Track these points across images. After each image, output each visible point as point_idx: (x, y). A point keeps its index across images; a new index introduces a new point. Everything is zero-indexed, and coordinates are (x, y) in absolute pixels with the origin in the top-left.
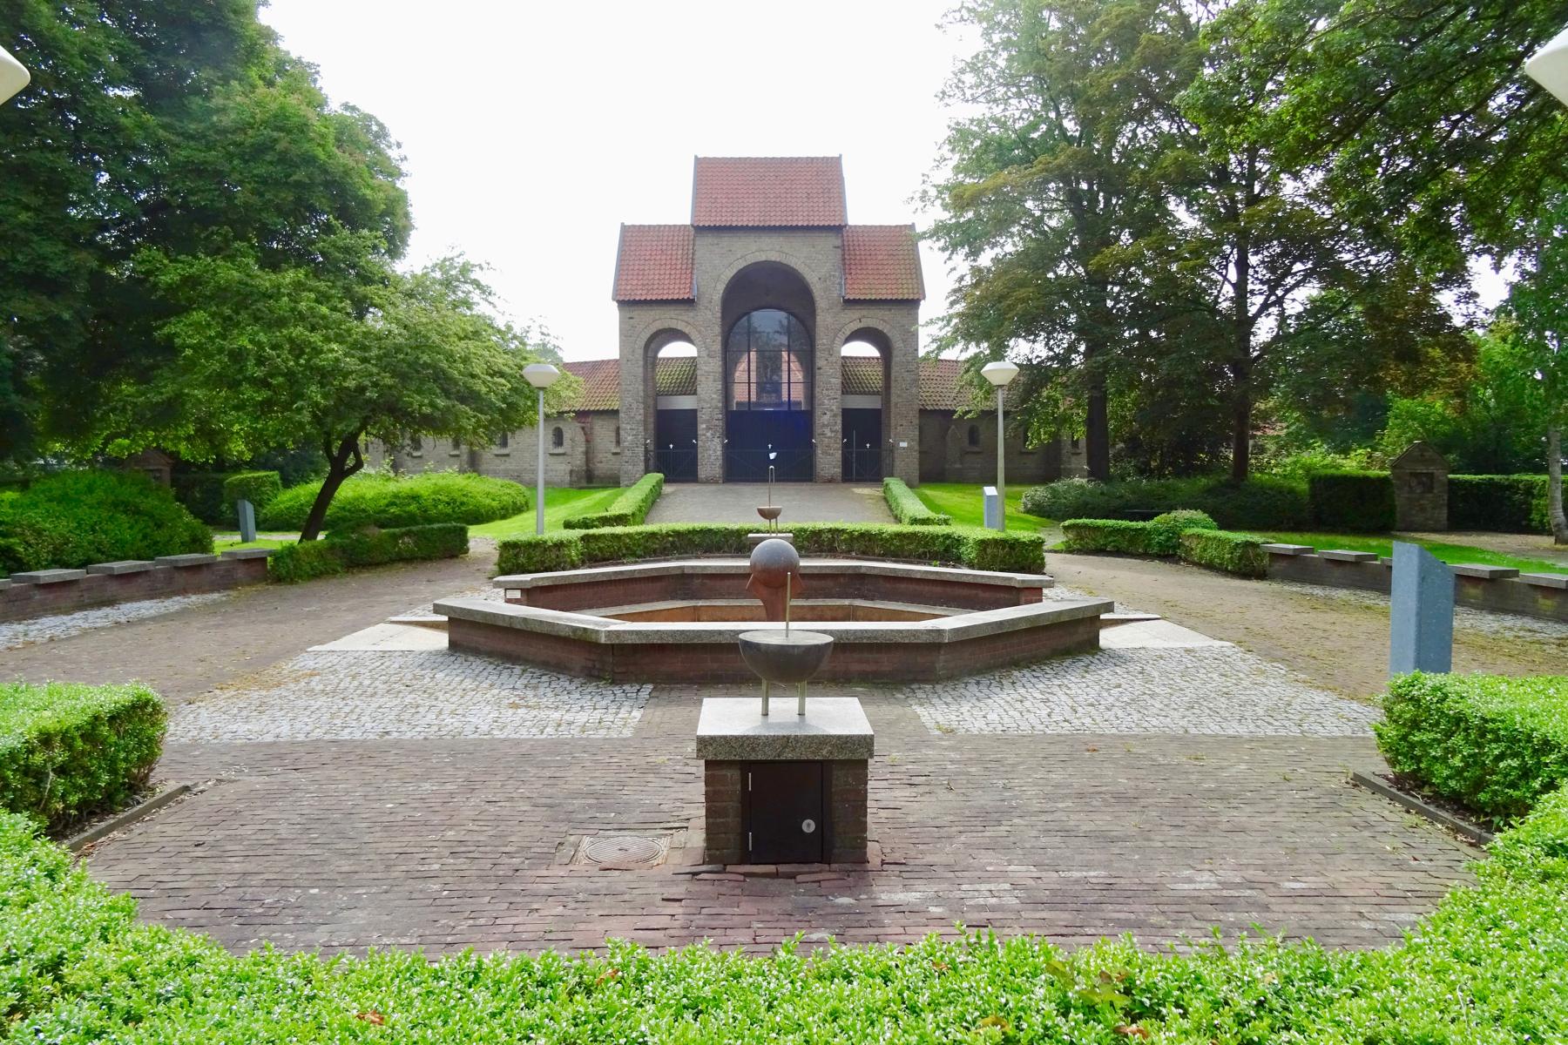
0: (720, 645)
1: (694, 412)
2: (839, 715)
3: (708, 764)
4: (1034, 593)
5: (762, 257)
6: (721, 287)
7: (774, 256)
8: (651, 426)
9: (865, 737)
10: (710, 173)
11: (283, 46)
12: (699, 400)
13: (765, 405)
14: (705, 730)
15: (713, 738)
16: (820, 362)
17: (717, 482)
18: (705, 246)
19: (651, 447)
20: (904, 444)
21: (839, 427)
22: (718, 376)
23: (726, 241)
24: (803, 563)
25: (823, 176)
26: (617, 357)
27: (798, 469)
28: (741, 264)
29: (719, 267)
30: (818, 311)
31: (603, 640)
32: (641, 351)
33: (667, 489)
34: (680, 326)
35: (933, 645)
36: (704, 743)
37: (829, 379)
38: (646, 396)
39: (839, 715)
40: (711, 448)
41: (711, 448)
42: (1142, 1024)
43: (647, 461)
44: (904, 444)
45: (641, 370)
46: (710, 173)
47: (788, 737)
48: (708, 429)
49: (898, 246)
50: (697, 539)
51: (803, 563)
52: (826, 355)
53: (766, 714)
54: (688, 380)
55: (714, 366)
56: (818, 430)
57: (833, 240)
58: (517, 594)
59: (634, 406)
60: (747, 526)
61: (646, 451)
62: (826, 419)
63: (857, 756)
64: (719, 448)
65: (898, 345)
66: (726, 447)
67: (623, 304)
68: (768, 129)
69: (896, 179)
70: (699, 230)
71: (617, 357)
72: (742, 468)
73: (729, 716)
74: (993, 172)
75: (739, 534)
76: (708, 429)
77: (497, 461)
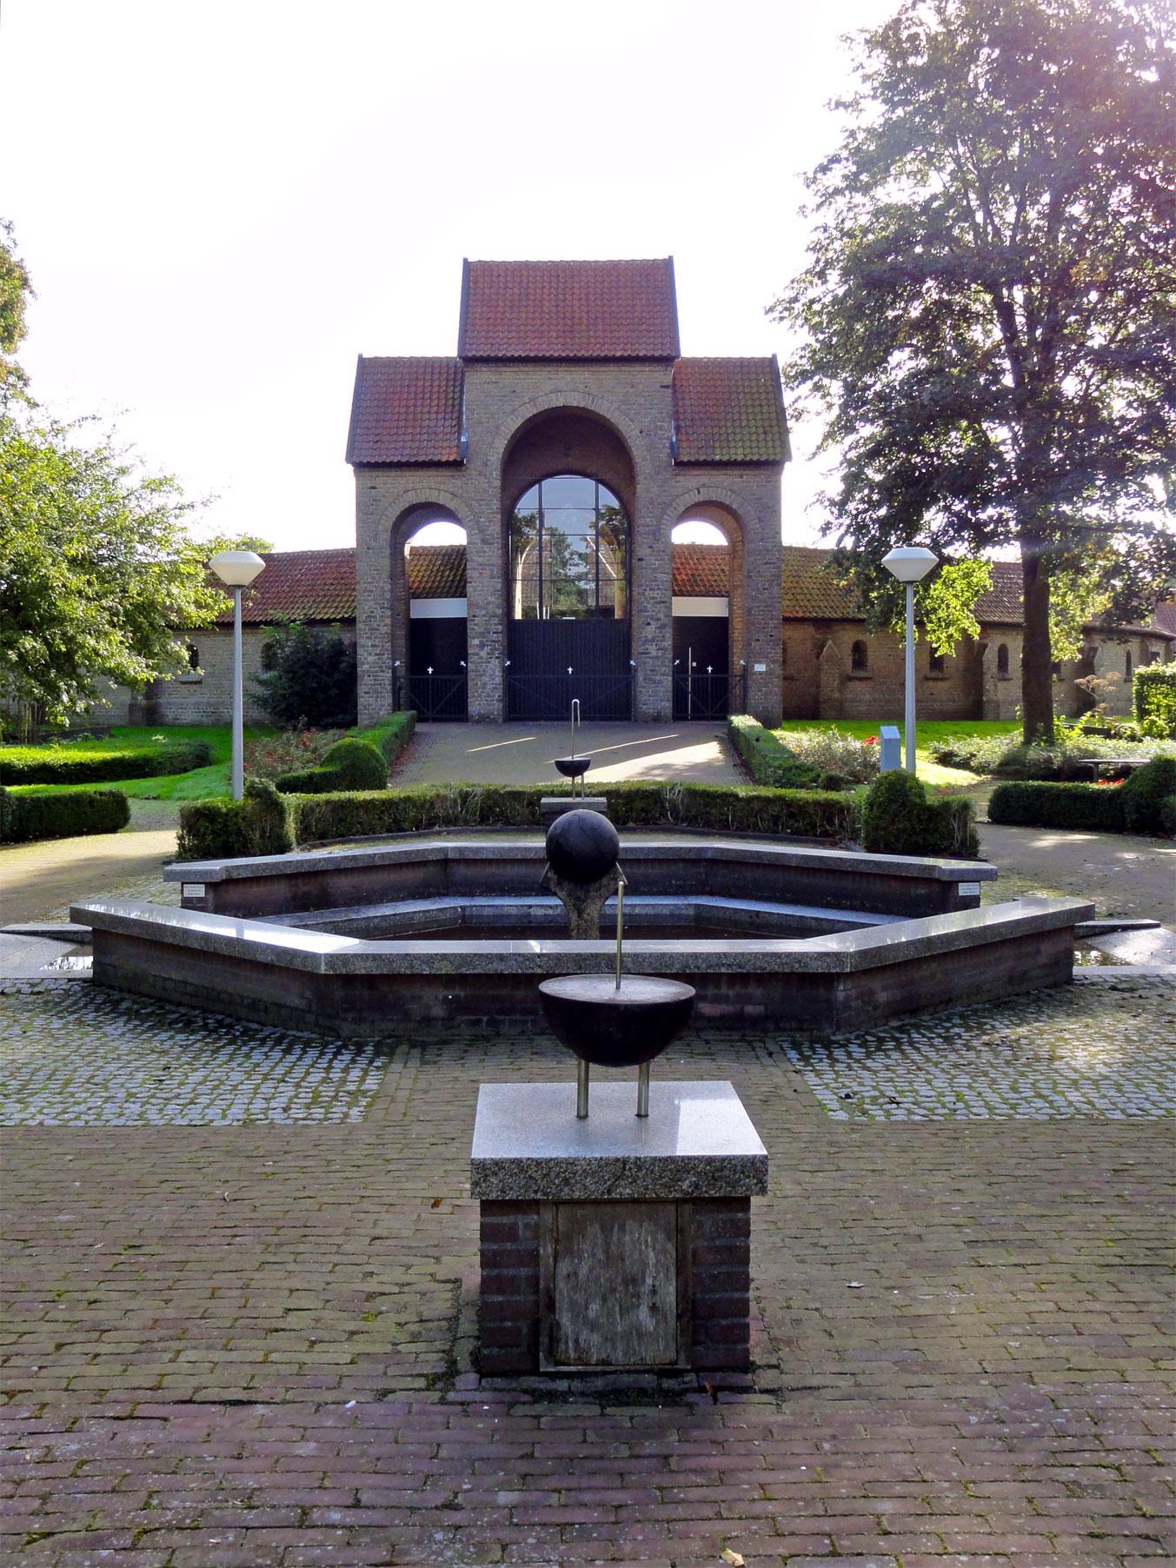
0: (501, 976)
1: (459, 625)
2: (710, 1120)
3: (488, 1207)
4: (942, 896)
5: (560, 402)
6: (501, 444)
7: (575, 400)
8: (402, 642)
9: (753, 1161)
10: (483, 282)
11: (199, 529)
12: (470, 605)
13: (563, 614)
14: (484, 1147)
15: (498, 1164)
16: (642, 550)
17: (494, 721)
18: (478, 380)
19: (402, 672)
20: (760, 668)
21: (668, 643)
22: (497, 571)
23: (509, 376)
24: (626, 842)
25: (650, 286)
26: (354, 545)
27: (614, 709)
28: (529, 411)
29: (503, 406)
30: (640, 478)
31: (323, 970)
32: (387, 536)
33: (419, 728)
34: (442, 499)
35: (811, 981)
36: (484, 1170)
37: (654, 572)
38: (394, 599)
39: (710, 1120)
40: (486, 674)
41: (486, 674)
42: (210, 616)
43: (396, 691)
44: (760, 668)
45: (387, 561)
46: (483, 282)
47: (625, 1161)
48: (482, 646)
49: (750, 391)
50: (733, 891)
51: (626, 842)
52: (650, 540)
53: (582, 1116)
54: (451, 571)
55: (493, 554)
56: (636, 647)
57: (664, 376)
58: (199, 891)
59: (378, 613)
60: (541, 785)
61: (395, 678)
62: (650, 631)
63: (739, 1192)
64: (498, 673)
65: (753, 525)
66: (508, 672)
67: (363, 466)
68: (569, 226)
69: (740, 304)
70: (469, 361)
71: (354, 545)
72: (528, 704)
73: (519, 1114)
74: (877, 285)
75: (532, 800)
76: (482, 646)
77: (184, 689)
